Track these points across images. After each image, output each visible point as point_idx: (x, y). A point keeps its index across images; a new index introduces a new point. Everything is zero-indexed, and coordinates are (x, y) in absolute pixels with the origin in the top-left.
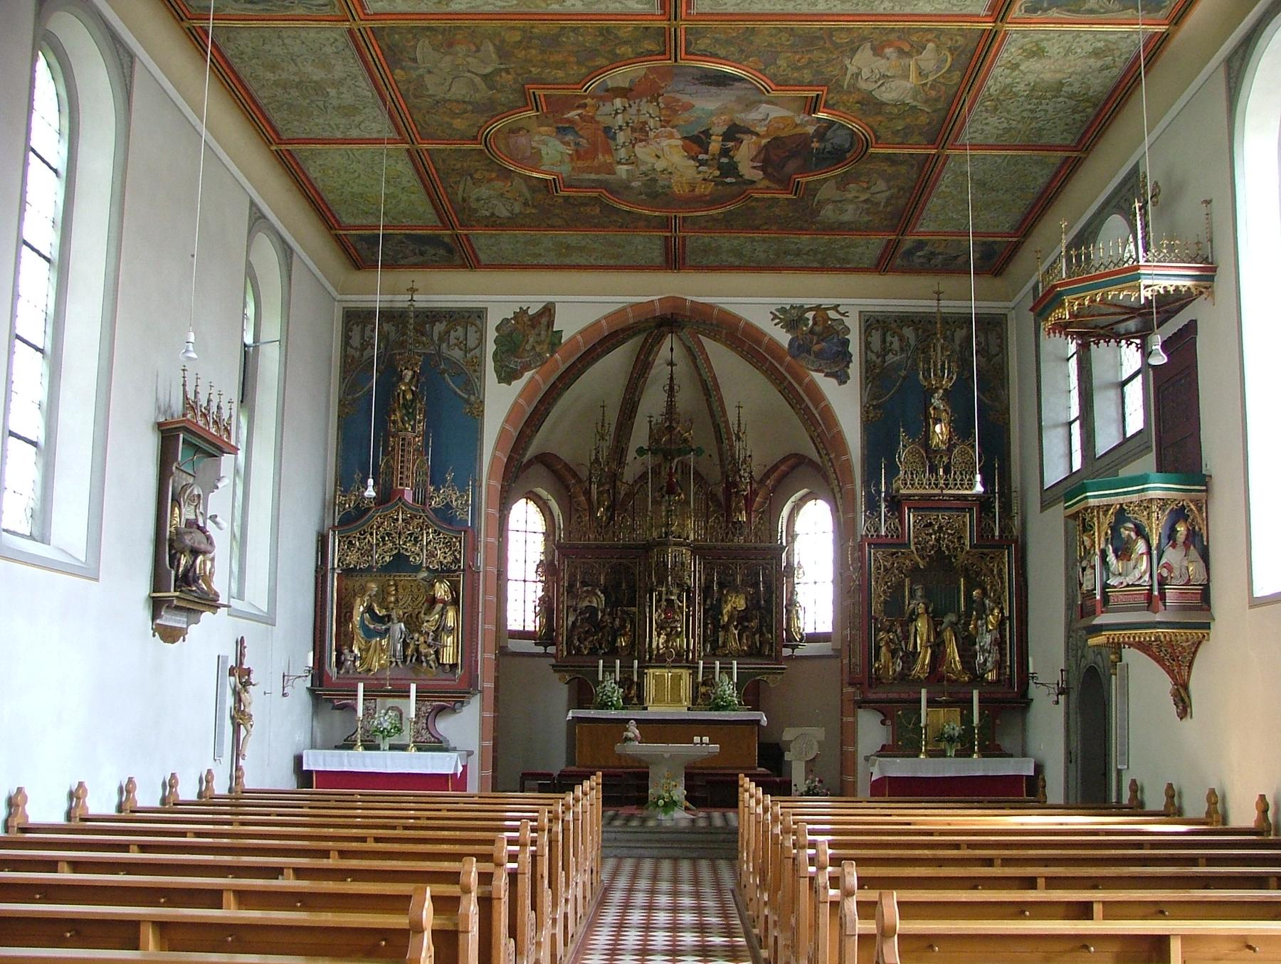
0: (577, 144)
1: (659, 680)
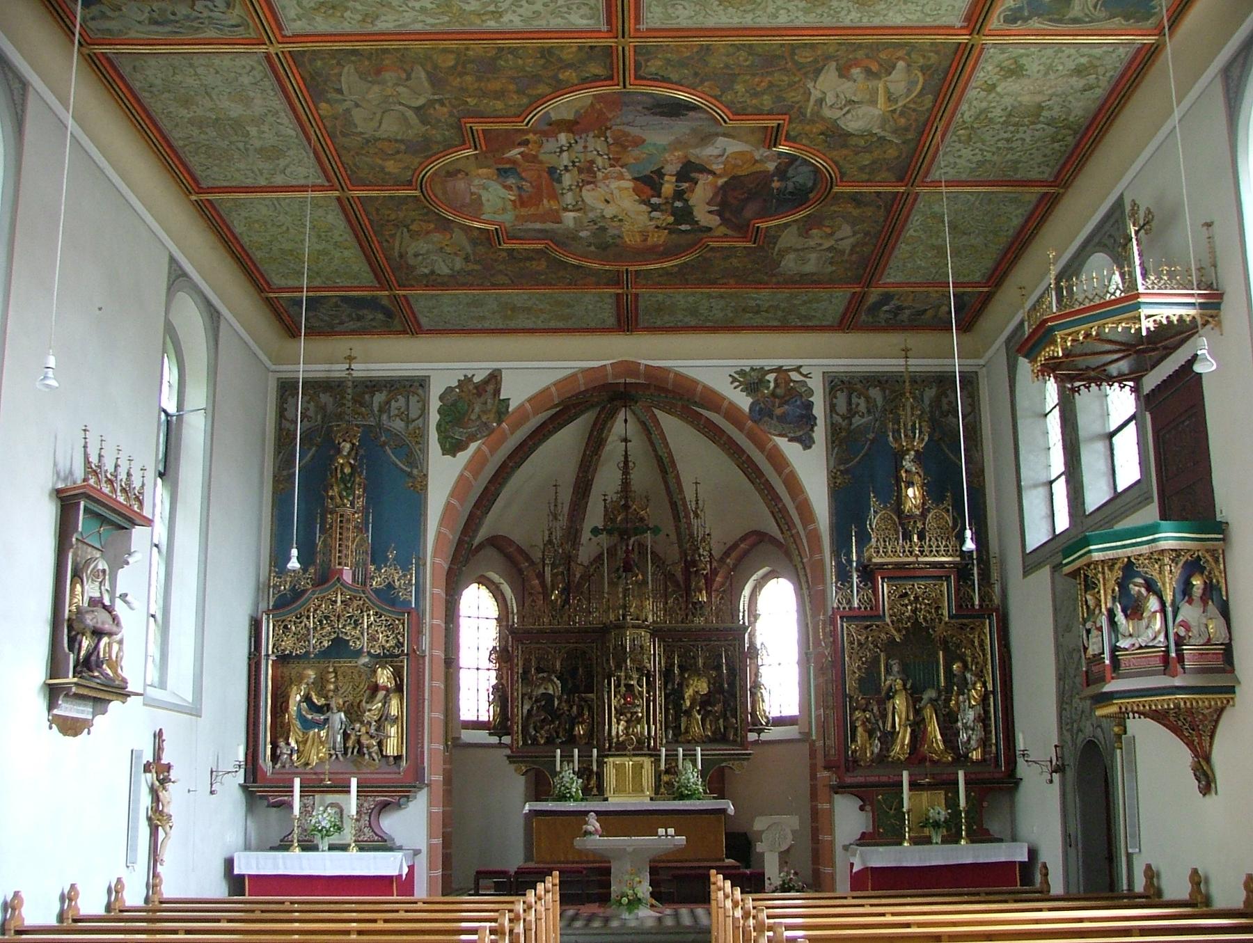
0: (519, 188)
1: (620, 769)
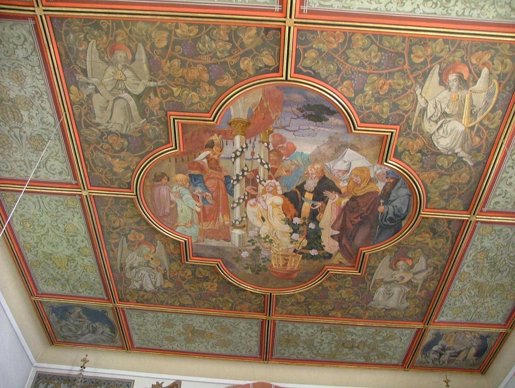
0: (204, 199)
